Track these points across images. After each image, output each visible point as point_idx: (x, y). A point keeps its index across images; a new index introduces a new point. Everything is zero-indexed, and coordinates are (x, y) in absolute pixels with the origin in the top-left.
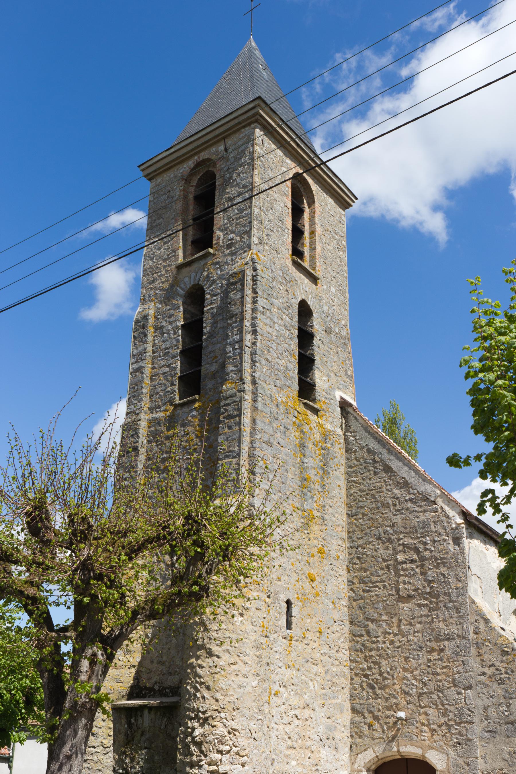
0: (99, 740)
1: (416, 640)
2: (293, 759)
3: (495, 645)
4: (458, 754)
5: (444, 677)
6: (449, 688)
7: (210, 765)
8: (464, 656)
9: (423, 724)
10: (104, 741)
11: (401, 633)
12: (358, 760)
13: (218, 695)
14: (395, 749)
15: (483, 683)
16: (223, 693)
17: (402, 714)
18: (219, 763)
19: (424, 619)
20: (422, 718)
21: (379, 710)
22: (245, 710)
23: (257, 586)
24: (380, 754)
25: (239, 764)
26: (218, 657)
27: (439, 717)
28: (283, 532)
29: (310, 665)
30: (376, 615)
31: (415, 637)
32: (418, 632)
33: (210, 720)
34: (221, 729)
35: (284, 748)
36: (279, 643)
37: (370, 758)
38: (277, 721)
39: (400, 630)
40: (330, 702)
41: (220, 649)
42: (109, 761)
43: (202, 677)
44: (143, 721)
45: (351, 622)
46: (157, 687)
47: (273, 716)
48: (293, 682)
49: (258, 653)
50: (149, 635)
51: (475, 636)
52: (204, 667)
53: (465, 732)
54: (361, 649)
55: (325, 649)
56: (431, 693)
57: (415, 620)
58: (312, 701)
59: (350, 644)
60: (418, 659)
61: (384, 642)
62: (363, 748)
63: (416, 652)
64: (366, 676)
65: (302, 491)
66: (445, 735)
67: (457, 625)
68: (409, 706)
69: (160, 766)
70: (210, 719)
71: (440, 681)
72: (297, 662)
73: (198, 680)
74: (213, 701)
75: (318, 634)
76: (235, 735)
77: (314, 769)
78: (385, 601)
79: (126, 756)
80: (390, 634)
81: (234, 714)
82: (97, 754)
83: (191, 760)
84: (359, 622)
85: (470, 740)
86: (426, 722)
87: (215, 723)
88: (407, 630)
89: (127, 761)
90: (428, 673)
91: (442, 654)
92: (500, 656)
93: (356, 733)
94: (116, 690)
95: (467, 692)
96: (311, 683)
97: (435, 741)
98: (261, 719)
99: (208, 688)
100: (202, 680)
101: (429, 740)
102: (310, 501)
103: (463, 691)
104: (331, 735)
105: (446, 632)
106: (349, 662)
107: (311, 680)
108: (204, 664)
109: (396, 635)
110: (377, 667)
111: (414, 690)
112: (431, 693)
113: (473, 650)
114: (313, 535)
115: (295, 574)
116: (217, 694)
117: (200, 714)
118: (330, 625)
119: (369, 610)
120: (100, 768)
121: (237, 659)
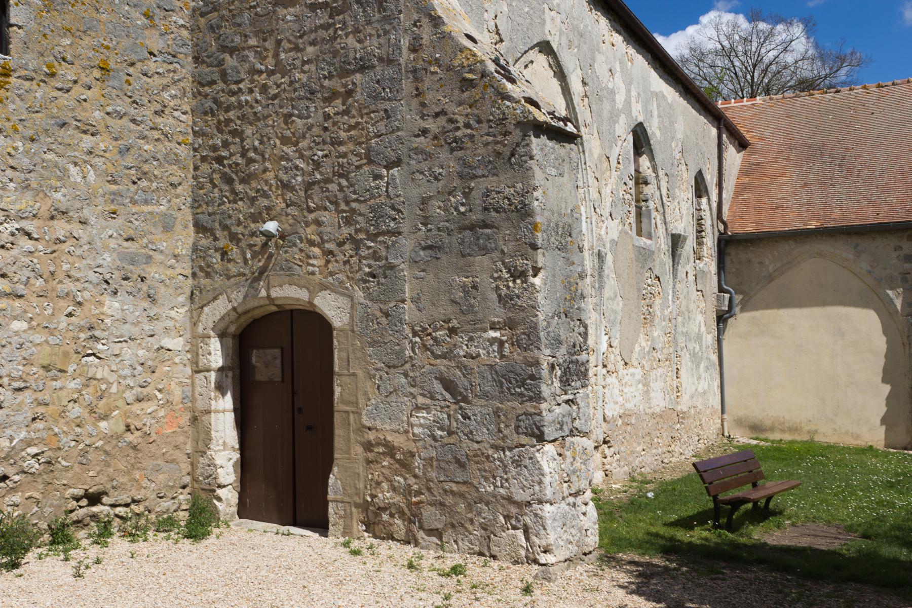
2: (15, 318)
3: (449, 69)
4: (369, 297)
5: (351, 146)
6: (358, 167)
8: (389, 99)
9: (312, 243)
11: (280, 69)
12: (203, 317)
14: (263, 293)
15: (423, 152)
17: (271, 226)
19: (322, 34)
21: (239, 223)
24: (239, 304)
27: (340, 227)
30: (237, 39)
31: (304, 72)
32: (309, 62)
37: (223, 312)
39: (278, 63)
40: (135, 209)
45: (196, 59)
48: (11, 161)
51: (412, 56)
54: (211, 109)
55: (122, 106)
57: (306, 37)
58: (78, 205)
59: (194, 103)
60: (309, 117)
61: (251, 91)
62: (211, 295)
63: (303, 104)
64: (220, 160)
66: (348, 261)
67: (379, 36)
71: (344, 155)
75: (97, 73)
77: (83, 336)
78: (254, 7)
80: (260, 72)
84: (208, 57)
85: (392, 267)
86: (316, 238)
88: (290, 62)
92: (457, 92)
93: (202, 269)
95: (391, 171)
96: (73, 170)
97: (332, 274)
101: (321, 273)
103: (385, 172)
104: (135, 271)
105: (358, 56)
106: (190, 138)
107: (76, 164)
109: (271, 73)
110: (238, 140)
111: (299, 179)
113: (407, 85)
118: (134, 57)
119: (227, 30)
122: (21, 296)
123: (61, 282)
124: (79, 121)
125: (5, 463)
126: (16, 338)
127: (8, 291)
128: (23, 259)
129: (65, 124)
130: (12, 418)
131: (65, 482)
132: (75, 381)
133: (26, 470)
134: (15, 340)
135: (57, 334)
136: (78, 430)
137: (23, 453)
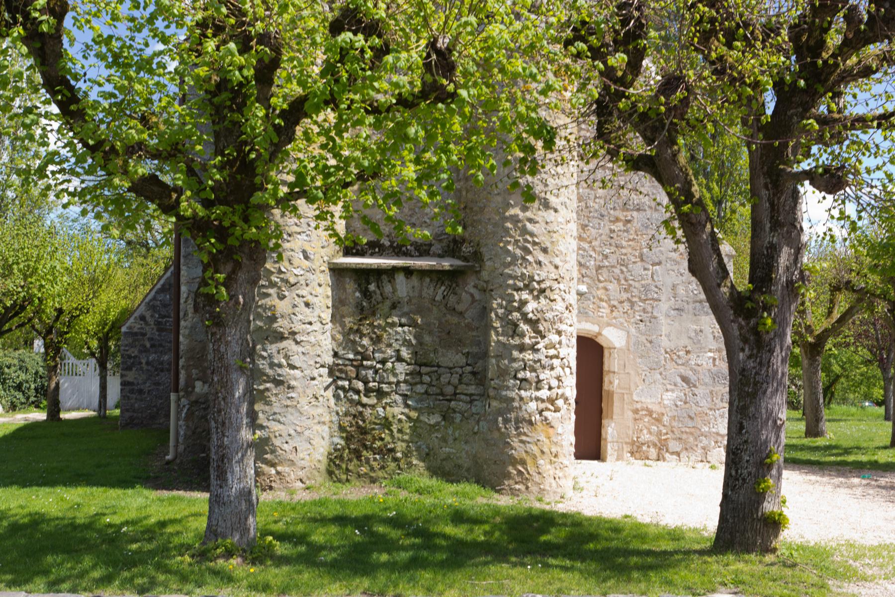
0: (316, 314)
1: (596, 207)
5: (630, 250)
9: (601, 300)
10: (322, 315)
13: (557, 261)
20: (600, 293)
26: (556, 211)
33: (548, 292)
43: (536, 236)
52: (537, 222)
53: (650, 310)
56: (613, 267)
63: (597, 221)
68: (585, 279)
74: (552, 269)
79: (362, 336)
85: (655, 318)
86: (606, 298)
89: (366, 342)
90: (610, 245)
91: (629, 225)
97: (615, 318)
99: (545, 250)
100: (536, 240)
103: (651, 267)
108: (537, 218)
112: (613, 267)
117: (535, 283)
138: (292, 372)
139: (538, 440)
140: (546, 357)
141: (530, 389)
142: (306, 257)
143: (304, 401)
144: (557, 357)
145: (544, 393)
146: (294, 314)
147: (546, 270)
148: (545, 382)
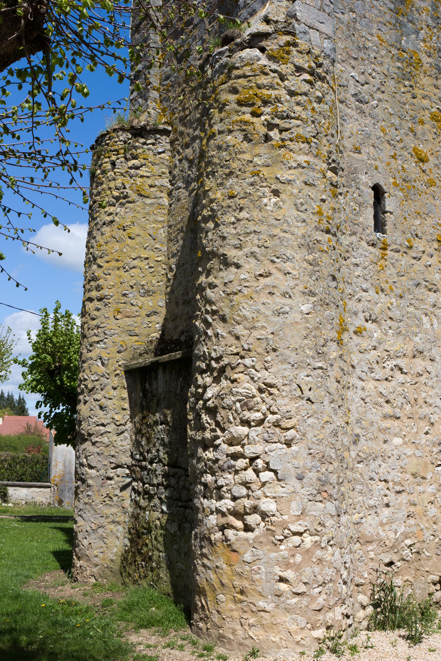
0: (109, 416)
2: (396, 435)
7: (231, 445)
10: (116, 417)
16: (248, 325)
18: (246, 441)
22: (287, 352)
23: (306, 145)
25: (279, 441)
26: (238, 266)
28: (362, 77)
29: (423, 290)
33: (228, 371)
34: (247, 385)
35: (377, 418)
36: (360, 251)
38: (363, 375)
41: (240, 253)
42: (125, 443)
44: (158, 386)
46: (183, 338)
47: (353, 367)
48: (390, 314)
49: (310, 257)
50: (173, 266)
52: (216, 286)
58: (429, 347)
65: (397, 19)
69: (177, 449)
70: (228, 369)
72: (398, 285)
73: (209, 308)
74: (232, 340)
76: (271, 394)
79: (143, 435)
81: (269, 358)
82: (109, 435)
83: (203, 438)
87: (236, 376)
94: (129, 346)
96: (425, 319)
98: (321, 368)
99: (223, 319)
100: (214, 308)
102: (413, 36)
107: (426, 315)
108: (216, 282)
114: (421, 92)
115: (388, 146)
116: (238, 327)
117: (213, 363)
120: (113, 453)
121: (271, 268)
122: (398, 418)
123: (421, 407)
124: (427, 281)
125: (392, 552)
126: (396, 451)
127: (391, 414)
128: (399, 389)
129: (419, 284)
130: (396, 515)
131: (427, 569)
132: (432, 487)
133: (405, 558)
134: (396, 452)
135: (420, 448)
136: (435, 526)
137: (403, 544)
138: (90, 471)
139: (217, 567)
140: (228, 455)
141: (212, 498)
142: (103, 364)
143: (98, 499)
144: (243, 456)
145: (227, 504)
146: (90, 417)
147: (223, 343)
148: (224, 489)
